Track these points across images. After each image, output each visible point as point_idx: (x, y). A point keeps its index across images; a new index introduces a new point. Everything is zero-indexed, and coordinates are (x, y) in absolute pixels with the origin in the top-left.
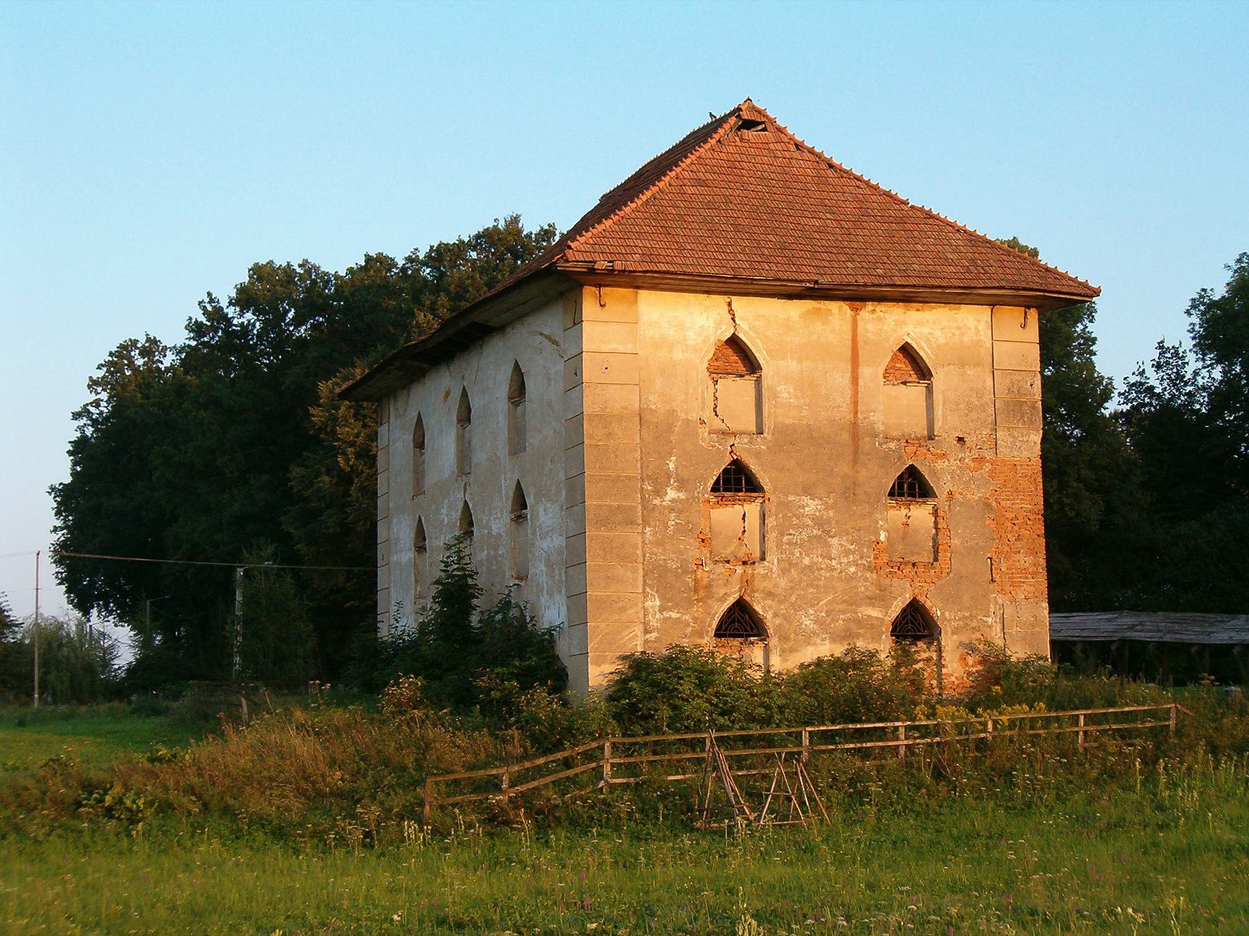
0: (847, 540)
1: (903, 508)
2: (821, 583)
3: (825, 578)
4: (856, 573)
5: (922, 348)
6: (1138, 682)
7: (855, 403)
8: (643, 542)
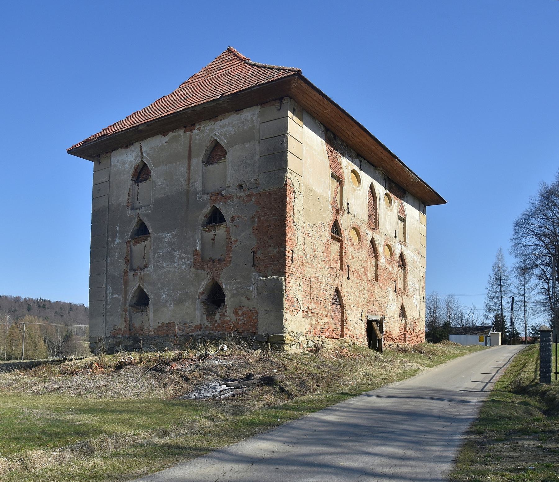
0: (181, 252)
1: (212, 231)
8: (399, 263)
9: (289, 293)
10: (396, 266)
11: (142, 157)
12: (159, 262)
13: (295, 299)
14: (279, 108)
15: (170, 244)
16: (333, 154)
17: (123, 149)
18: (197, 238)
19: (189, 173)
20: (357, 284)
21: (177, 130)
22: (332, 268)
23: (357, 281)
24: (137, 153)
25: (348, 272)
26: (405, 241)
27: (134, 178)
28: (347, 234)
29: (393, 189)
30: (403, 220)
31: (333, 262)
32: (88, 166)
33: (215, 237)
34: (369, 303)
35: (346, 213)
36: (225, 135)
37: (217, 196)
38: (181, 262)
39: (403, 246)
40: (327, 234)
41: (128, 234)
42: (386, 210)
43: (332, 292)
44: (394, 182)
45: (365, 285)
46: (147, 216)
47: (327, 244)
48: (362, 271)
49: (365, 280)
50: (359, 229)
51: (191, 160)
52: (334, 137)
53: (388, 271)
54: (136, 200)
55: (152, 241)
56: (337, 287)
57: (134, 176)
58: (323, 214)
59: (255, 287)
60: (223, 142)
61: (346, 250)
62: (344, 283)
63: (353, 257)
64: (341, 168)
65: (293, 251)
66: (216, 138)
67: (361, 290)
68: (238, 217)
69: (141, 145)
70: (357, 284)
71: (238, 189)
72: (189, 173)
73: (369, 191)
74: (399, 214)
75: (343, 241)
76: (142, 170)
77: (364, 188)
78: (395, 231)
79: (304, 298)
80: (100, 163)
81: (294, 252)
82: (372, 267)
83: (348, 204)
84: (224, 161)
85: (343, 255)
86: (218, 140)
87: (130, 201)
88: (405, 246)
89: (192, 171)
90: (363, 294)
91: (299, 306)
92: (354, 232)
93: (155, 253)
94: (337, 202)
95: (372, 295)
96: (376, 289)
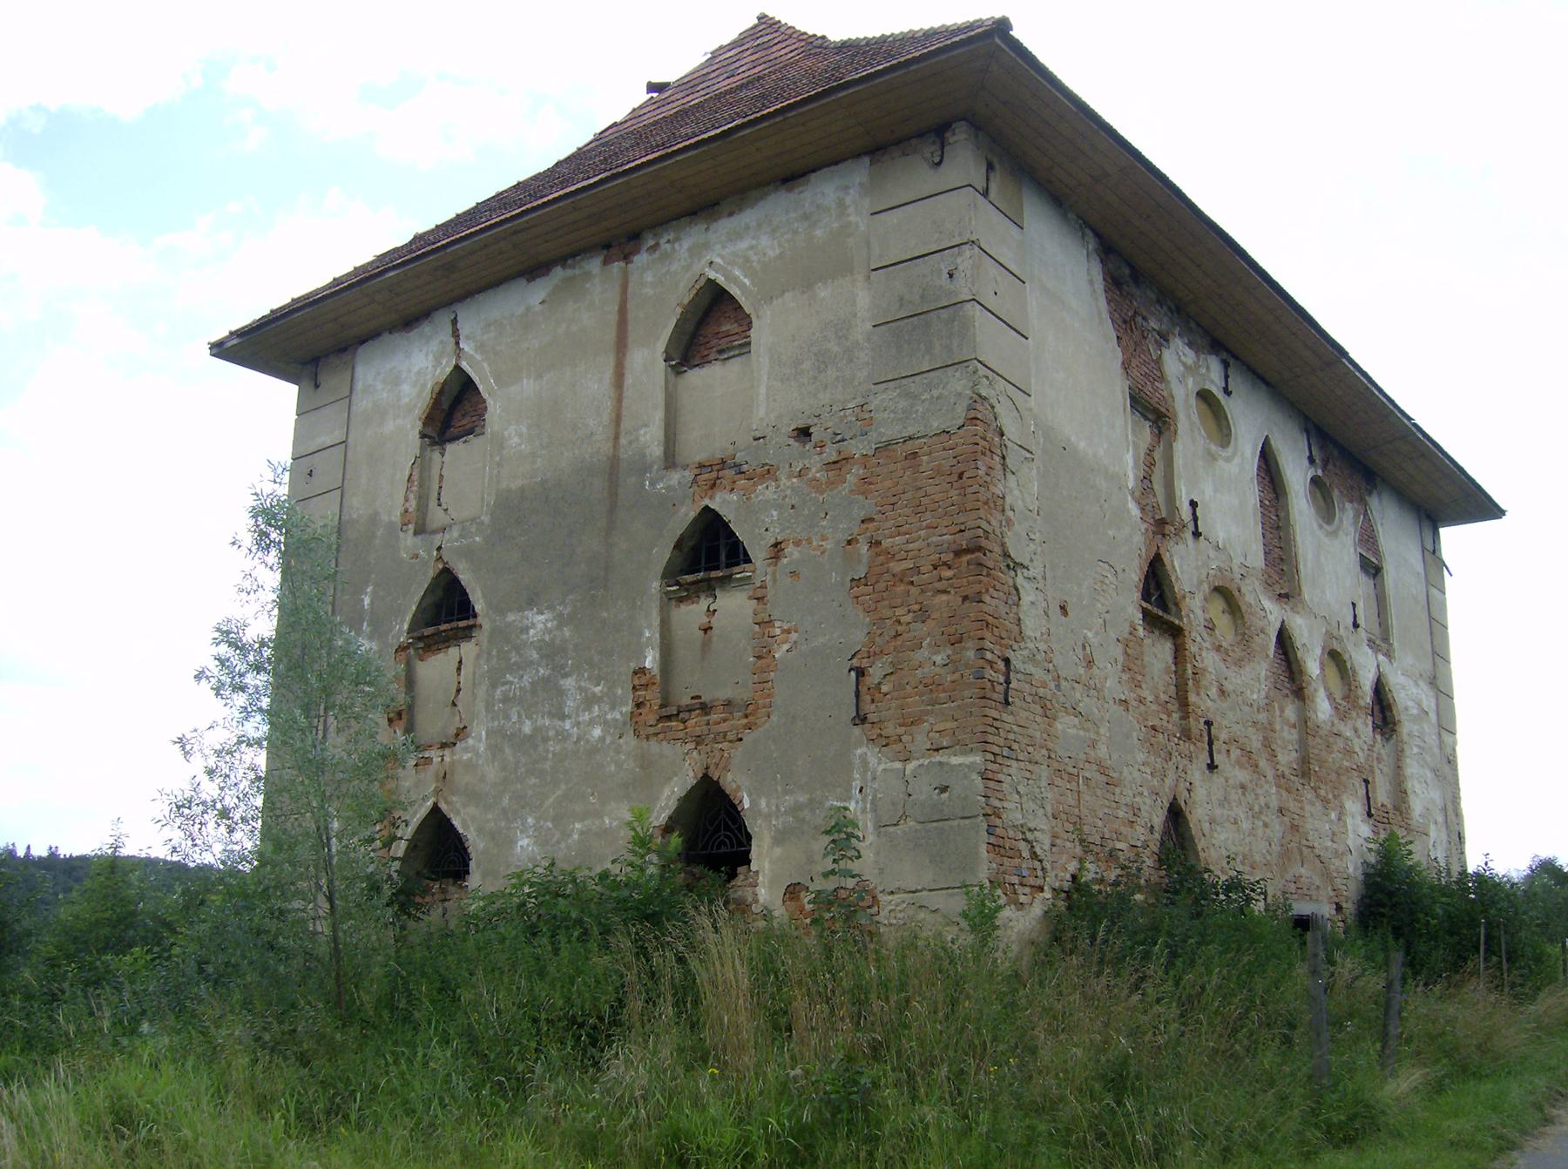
0: (589, 678)
2: (547, 766)
3: (554, 754)
4: (602, 739)
5: (736, 281)
6: (88, 1141)
7: (618, 420)
9: (998, 822)
10: (1365, 725)
11: (458, 357)
12: (508, 718)
13: (1022, 846)
14: (937, 160)
15: (552, 652)
16: (1132, 330)
17: (396, 335)
18: (645, 625)
19: (619, 400)
20: (1243, 787)
21: (578, 258)
22: (1154, 728)
23: (1242, 775)
24: (441, 342)
25: (1210, 743)
26: (1386, 639)
27: (429, 431)
28: (1196, 609)
29: (1335, 465)
30: (1372, 569)
31: (1154, 707)
32: (281, 396)
33: (715, 621)
34: (1285, 854)
35: (1188, 535)
36: (746, 264)
37: (718, 471)
38: (587, 716)
39: (1381, 657)
40: (1130, 606)
41: (402, 622)
42: (1319, 533)
43: (1159, 818)
44: (1336, 444)
45: (1271, 794)
46: (468, 553)
47: (1129, 643)
48: (1255, 742)
49: (1270, 774)
50: (1236, 594)
51: (624, 355)
52: (1131, 275)
53: (1340, 743)
54: (433, 503)
55: (485, 645)
56: (1175, 798)
57: (429, 420)
58: (1110, 533)
59: (864, 800)
60: (739, 286)
61: (1196, 664)
62: (1197, 783)
63: (1222, 692)
64: (1162, 378)
65: (1007, 661)
66: (712, 275)
67: (1256, 808)
68: (797, 543)
69: (455, 318)
70: (1243, 787)
71: (797, 444)
72: (619, 400)
73: (1259, 468)
74: (1359, 550)
75: (1186, 633)
76: (457, 401)
77: (1242, 455)
78: (1354, 604)
79: (1058, 842)
80: (317, 386)
81: (1012, 667)
82: (1286, 728)
83: (1193, 504)
84: (742, 351)
85: (1190, 683)
86: (721, 280)
87: (412, 505)
88: (1389, 655)
89: (628, 393)
90: (1266, 825)
91: (1040, 873)
92: (1218, 604)
93: (494, 686)
94: (1155, 496)
95: (1295, 828)
96: (1308, 808)
